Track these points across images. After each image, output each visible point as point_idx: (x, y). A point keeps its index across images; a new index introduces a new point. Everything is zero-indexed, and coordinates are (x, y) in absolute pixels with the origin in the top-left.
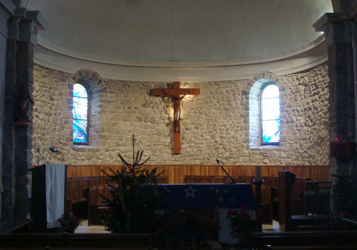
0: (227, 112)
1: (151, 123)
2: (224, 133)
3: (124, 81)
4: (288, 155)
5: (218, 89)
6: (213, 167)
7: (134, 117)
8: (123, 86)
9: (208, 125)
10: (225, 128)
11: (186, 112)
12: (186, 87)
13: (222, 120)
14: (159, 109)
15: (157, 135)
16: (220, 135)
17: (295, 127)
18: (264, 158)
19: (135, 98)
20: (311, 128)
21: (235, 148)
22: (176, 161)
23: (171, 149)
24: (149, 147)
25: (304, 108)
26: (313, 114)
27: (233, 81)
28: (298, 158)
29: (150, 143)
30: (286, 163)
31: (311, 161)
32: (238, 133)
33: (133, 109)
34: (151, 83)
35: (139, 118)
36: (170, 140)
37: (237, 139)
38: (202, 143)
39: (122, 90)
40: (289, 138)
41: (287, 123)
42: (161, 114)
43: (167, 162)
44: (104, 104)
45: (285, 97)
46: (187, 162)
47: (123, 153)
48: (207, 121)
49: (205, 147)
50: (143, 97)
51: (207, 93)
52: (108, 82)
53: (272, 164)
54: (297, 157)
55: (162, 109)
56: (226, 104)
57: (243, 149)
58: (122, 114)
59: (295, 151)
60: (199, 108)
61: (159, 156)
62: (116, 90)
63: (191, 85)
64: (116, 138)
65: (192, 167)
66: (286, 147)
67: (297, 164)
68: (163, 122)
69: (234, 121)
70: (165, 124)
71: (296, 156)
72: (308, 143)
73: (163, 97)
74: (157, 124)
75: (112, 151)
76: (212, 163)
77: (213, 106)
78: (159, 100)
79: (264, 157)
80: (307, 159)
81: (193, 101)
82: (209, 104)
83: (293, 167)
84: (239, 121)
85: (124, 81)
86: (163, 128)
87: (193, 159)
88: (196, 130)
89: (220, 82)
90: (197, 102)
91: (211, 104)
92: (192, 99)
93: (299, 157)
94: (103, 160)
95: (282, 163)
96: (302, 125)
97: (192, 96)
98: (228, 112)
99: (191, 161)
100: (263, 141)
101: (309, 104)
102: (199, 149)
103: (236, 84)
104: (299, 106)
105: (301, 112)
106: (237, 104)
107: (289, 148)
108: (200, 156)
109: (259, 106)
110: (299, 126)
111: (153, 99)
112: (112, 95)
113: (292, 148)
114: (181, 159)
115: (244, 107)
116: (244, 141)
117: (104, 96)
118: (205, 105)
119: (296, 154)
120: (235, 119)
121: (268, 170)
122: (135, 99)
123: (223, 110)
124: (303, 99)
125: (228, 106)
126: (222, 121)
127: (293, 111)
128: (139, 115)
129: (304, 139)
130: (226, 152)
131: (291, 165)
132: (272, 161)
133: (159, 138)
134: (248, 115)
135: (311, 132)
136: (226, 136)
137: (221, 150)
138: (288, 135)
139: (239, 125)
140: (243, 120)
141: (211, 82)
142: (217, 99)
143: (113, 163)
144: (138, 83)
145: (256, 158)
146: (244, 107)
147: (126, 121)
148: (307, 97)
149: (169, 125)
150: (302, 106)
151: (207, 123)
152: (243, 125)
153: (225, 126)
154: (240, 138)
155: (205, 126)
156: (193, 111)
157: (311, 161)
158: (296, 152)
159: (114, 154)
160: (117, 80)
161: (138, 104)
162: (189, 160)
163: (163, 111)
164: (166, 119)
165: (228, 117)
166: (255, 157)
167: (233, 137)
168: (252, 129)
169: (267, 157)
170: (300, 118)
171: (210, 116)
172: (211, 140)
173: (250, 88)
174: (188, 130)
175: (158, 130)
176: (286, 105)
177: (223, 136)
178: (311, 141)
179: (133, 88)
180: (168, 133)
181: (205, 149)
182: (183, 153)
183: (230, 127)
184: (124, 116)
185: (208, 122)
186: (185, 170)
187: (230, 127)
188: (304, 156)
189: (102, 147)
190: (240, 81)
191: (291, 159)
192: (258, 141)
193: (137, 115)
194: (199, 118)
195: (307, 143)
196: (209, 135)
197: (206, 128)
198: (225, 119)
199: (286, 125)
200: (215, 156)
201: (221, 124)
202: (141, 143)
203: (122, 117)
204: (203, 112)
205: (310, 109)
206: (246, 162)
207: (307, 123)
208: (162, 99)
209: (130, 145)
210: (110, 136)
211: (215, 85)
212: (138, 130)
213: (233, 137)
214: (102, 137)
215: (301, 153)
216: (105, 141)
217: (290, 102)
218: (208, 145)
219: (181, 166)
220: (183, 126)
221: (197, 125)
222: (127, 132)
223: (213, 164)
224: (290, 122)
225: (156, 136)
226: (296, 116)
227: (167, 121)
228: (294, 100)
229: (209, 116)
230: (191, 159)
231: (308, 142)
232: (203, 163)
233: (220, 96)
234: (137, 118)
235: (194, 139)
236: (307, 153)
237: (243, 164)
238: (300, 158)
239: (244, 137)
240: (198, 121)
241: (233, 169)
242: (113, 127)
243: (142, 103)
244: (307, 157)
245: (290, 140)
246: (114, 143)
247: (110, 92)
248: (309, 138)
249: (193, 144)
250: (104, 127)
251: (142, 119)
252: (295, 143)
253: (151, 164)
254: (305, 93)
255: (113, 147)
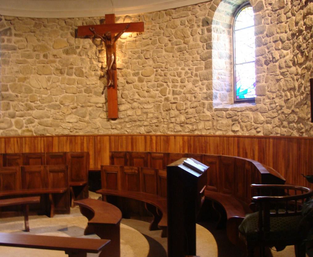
0: (182, 54)
1: (76, 76)
2: (178, 87)
3: (37, 19)
4: (267, 118)
5: (170, 20)
6: (162, 138)
7: (52, 68)
8: (36, 25)
9: (156, 75)
10: (180, 78)
11: (126, 58)
12: (128, 21)
13: (176, 67)
14: (88, 56)
15: (86, 93)
16: (173, 89)
17: (278, 69)
18: (234, 124)
19: (55, 42)
20: (302, 68)
21: (193, 108)
22: (113, 129)
23: (106, 111)
24: (74, 110)
25: (291, 32)
26: (304, 41)
27: (189, 7)
28: (282, 123)
29: (76, 105)
30: (265, 132)
31: (302, 128)
32: (197, 85)
33: (51, 58)
34: (77, 19)
35: (59, 69)
36: (104, 99)
37: (196, 94)
38: (148, 102)
39: (34, 32)
40: (269, 89)
41: (267, 63)
42: (91, 63)
43: (100, 131)
44: (6, 51)
45: (263, 21)
46: (128, 131)
47: (36, 119)
48: (155, 70)
49: (152, 108)
50: (65, 39)
51: (155, 29)
52: (12, 22)
53: (245, 132)
54: (281, 122)
55: (93, 55)
56: (180, 42)
57: (203, 110)
58: (36, 65)
59: (277, 112)
60: (143, 50)
61: (90, 123)
62: (25, 32)
63: (133, 19)
64: (26, 99)
65: (134, 137)
66: (265, 104)
67: (281, 135)
68: (95, 74)
69: (192, 66)
70: (97, 77)
71: (279, 119)
72: (298, 95)
73: (94, 39)
74: (86, 78)
75: (20, 117)
76: (161, 131)
77: (162, 46)
78: (89, 43)
79: (234, 122)
80: (295, 126)
81: (136, 41)
82: (157, 45)
83: (274, 138)
84: (199, 66)
85: (37, 18)
86: (94, 83)
87: (136, 125)
88: (140, 84)
89: (173, 10)
90: (141, 42)
91: (160, 44)
92: (135, 39)
93: (284, 120)
94: (7, 130)
95: (258, 132)
96: (287, 64)
97: (134, 34)
98: (184, 53)
99: (133, 129)
100: (236, 98)
101: (299, 24)
102: (145, 110)
103: (194, 10)
104: (284, 31)
105: (287, 42)
106: (195, 41)
107: (269, 106)
108: (146, 121)
109: (230, 42)
110: (284, 66)
111: (79, 42)
112: (18, 38)
113: (273, 106)
114: (119, 126)
115: (205, 44)
116: (206, 96)
117: (6, 40)
118: (153, 46)
119: (279, 117)
120: (193, 63)
121: (238, 143)
122: (53, 43)
123: (176, 52)
124: (290, 18)
125: (183, 46)
126: (175, 67)
127: (275, 42)
128: (59, 65)
129: (291, 89)
130: (181, 115)
131: (271, 135)
132: (245, 129)
133: (88, 96)
134: (210, 57)
135: (302, 74)
136: (180, 91)
137: (174, 113)
138: (268, 84)
139: (198, 73)
140: (204, 64)
141: (159, 11)
142: (169, 35)
143: (21, 133)
144: (58, 20)
145: (222, 123)
146: (205, 44)
147: (40, 75)
148: (295, 13)
149: (102, 78)
150: (288, 30)
151: (155, 73)
152: (204, 71)
153: (179, 75)
154: (201, 92)
155: (153, 77)
156: (136, 56)
157: (302, 128)
158: (280, 112)
159: (24, 121)
160: (27, 18)
161: (58, 50)
162: (131, 127)
163: (94, 58)
164: (99, 69)
165: (182, 62)
166: (220, 122)
167: (190, 92)
168: (218, 79)
169: (237, 122)
170: (285, 52)
171: (159, 61)
172: (161, 97)
173: (214, 14)
174: (129, 83)
175: (88, 86)
176: (265, 33)
177: (177, 90)
178: (302, 92)
179: (51, 28)
180: (101, 90)
181: (152, 110)
182: (121, 117)
183: (186, 76)
184: (37, 68)
185: (156, 71)
186: (124, 142)
187: (186, 76)
188: (290, 120)
189: (3, 112)
190: (200, 5)
191: (272, 124)
192: (230, 96)
193: (56, 65)
194: (144, 65)
195: (296, 96)
196: (157, 90)
197: (153, 79)
198: (179, 65)
199: (265, 67)
200: (165, 120)
201: (174, 73)
202: (62, 104)
203: (35, 69)
204: (149, 57)
205: (300, 32)
206: (208, 129)
207: (296, 60)
208: (93, 42)
209: (46, 108)
210: (17, 96)
211: (165, 15)
212: (59, 87)
213: (190, 91)
214: (3, 97)
215: (286, 114)
216: (9, 103)
217: (271, 26)
218: (156, 104)
219: (119, 136)
220: (122, 78)
221: (142, 76)
222: (42, 89)
223: (163, 134)
224: (270, 61)
225: (84, 94)
226: (279, 50)
227: (100, 73)
228: (276, 22)
229: (158, 62)
230: (134, 126)
231: (298, 94)
232: (150, 131)
233: (172, 30)
234: (57, 69)
235: (137, 96)
236: (296, 115)
237: (204, 134)
238: (285, 123)
239: (205, 91)
240: (142, 70)
241: (189, 141)
242: (21, 83)
243: (64, 48)
244: (295, 121)
245: (270, 92)
246: (22, 105)
247: (16, 35)
248: (300, 87)
249: (135, 104)
250: (5, 84)
251: (64, 71)
252: (278, 97)
253: (77, 134)
254: (293, 5)
255: (22, 112)
